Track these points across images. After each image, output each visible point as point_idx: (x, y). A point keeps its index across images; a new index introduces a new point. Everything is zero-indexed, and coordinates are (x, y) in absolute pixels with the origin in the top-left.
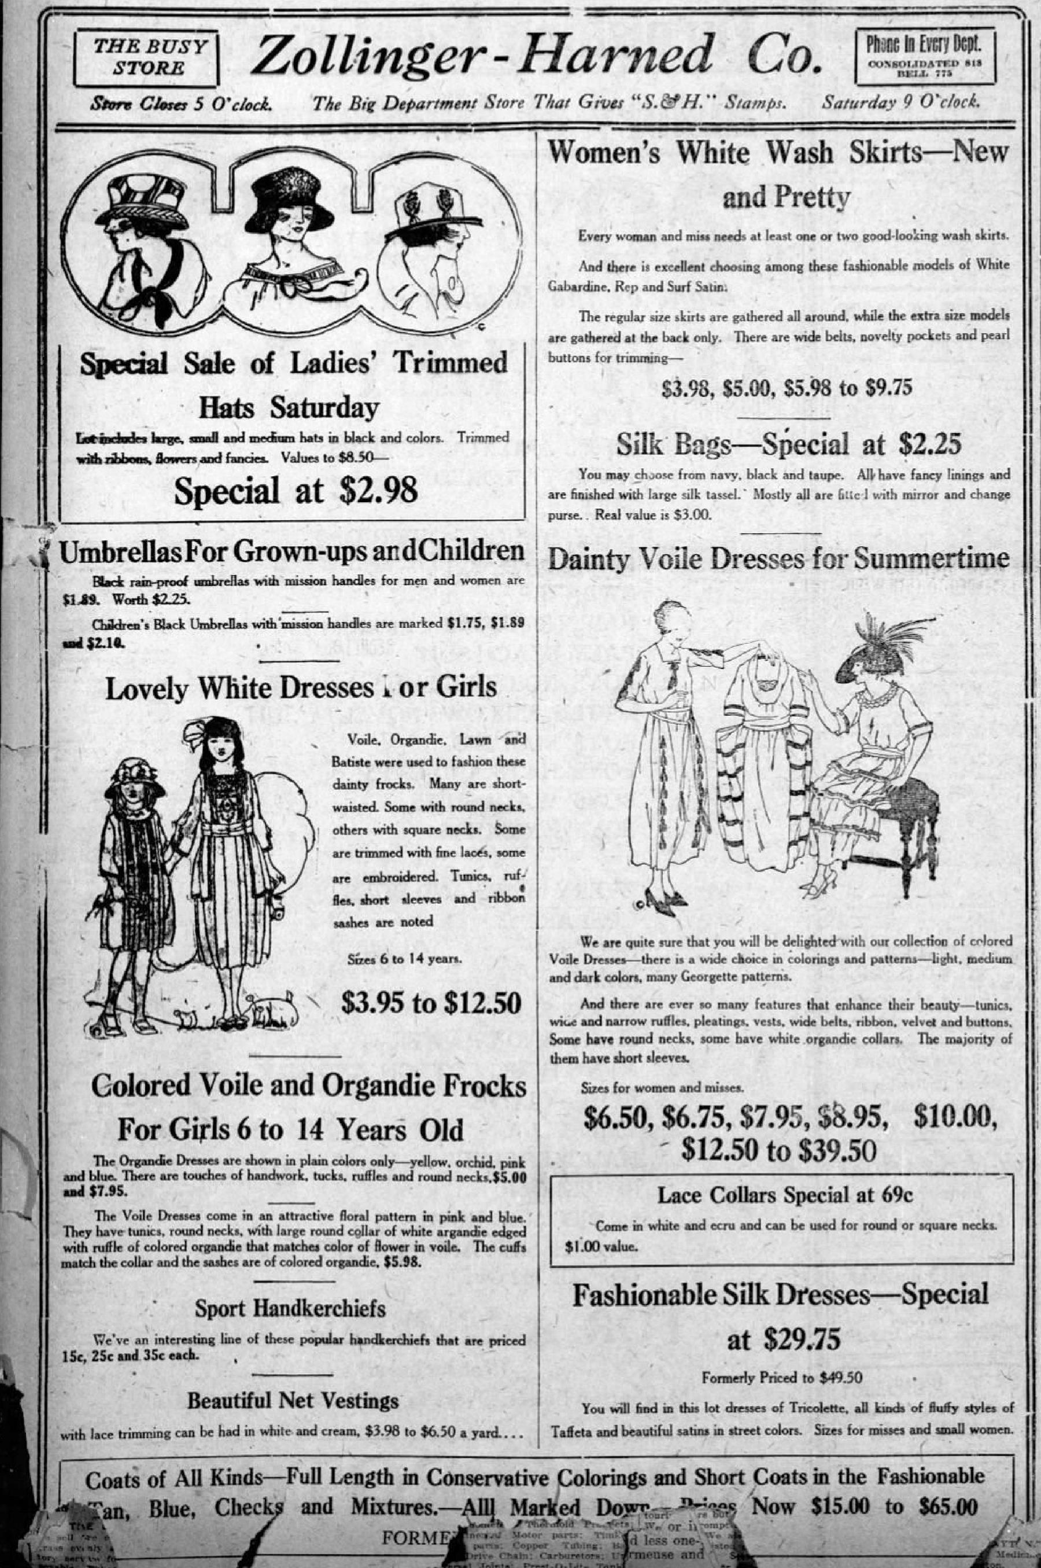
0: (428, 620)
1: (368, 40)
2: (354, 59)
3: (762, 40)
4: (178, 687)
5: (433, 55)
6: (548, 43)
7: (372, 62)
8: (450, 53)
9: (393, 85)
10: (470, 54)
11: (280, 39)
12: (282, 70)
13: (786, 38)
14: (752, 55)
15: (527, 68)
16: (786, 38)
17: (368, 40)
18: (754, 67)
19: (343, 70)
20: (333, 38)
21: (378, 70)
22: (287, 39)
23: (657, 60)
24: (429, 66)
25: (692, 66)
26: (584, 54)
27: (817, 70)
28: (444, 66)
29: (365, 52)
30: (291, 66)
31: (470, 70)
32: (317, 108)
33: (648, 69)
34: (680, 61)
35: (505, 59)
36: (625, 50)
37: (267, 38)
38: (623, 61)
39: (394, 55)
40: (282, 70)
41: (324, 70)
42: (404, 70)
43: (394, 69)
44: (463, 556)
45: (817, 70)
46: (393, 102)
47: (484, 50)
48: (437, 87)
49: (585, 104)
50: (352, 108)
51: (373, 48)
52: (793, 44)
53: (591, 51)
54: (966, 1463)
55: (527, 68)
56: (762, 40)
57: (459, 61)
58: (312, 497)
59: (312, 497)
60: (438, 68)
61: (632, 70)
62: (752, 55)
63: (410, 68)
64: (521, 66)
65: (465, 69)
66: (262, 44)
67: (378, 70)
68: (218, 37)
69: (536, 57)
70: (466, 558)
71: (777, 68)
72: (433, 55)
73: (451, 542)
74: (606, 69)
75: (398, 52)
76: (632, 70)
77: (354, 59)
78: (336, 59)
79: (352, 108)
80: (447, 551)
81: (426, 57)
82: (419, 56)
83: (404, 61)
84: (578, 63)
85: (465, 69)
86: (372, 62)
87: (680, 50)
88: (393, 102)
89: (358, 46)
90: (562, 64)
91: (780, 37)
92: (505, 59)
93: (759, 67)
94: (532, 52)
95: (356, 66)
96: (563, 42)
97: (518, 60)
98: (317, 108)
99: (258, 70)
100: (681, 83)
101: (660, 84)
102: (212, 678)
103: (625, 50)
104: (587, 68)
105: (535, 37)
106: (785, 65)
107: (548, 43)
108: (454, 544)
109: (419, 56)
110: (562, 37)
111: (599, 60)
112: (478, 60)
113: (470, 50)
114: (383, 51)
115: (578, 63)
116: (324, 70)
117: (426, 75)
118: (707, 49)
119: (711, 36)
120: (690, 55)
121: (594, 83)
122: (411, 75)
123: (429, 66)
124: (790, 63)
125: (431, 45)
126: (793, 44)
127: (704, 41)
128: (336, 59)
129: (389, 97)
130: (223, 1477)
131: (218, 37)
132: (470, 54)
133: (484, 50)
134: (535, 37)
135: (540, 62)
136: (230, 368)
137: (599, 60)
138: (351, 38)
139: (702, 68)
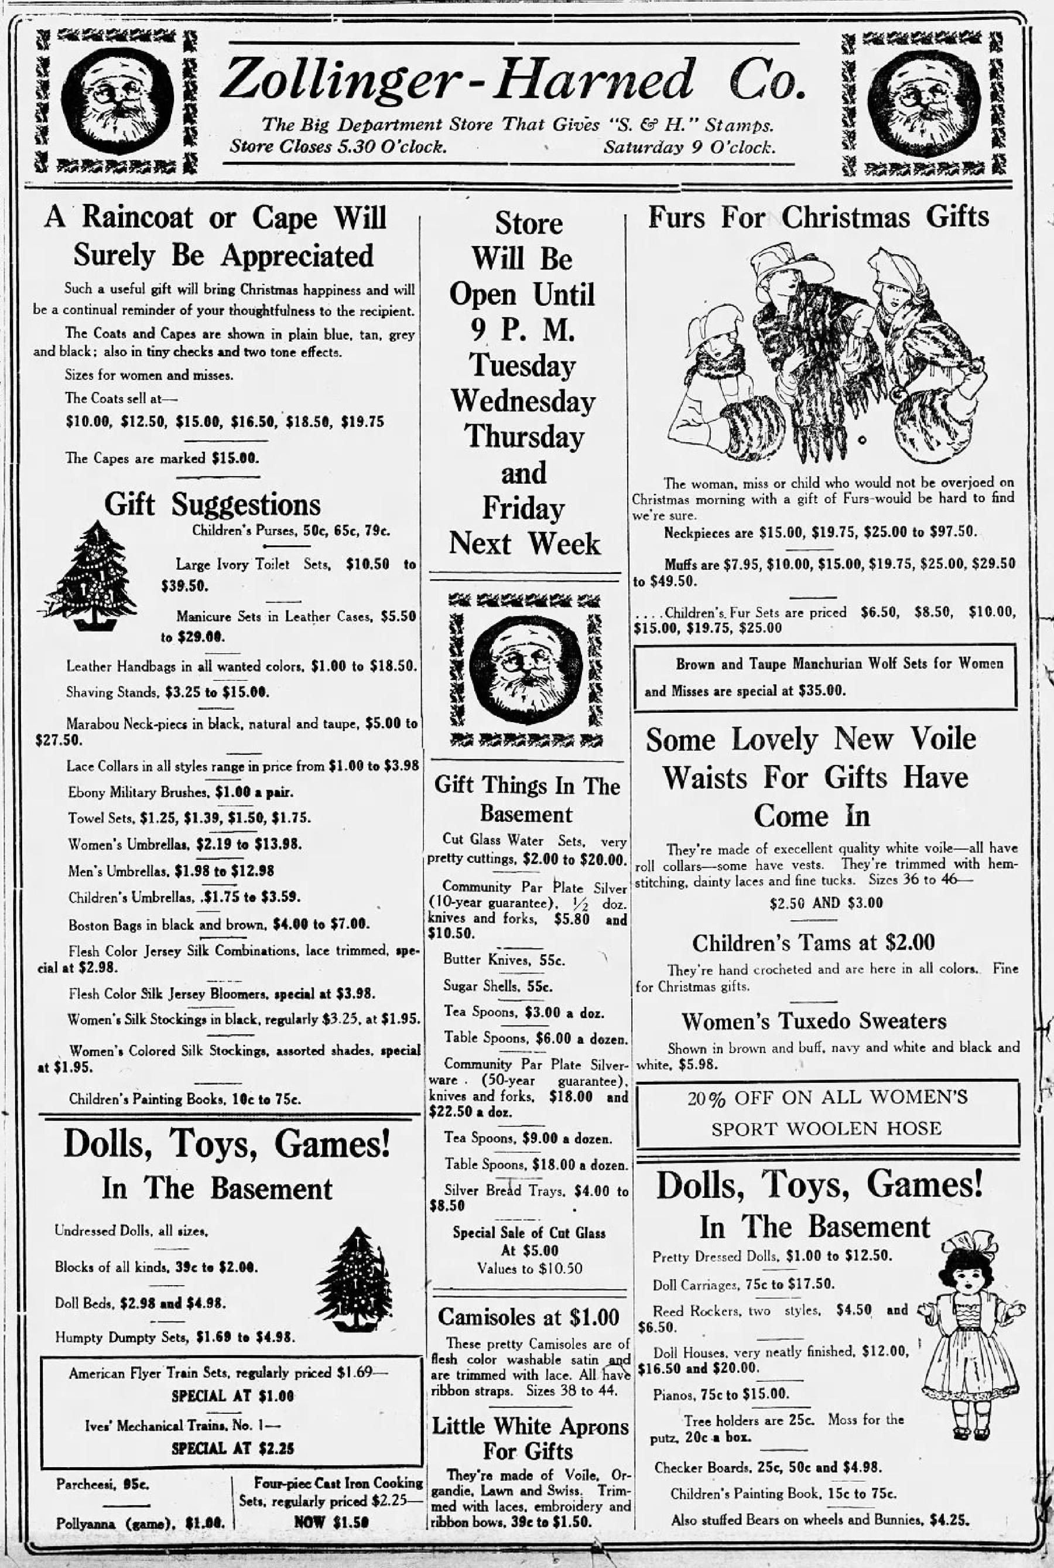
0: (837, 1348)
1: (339, 64)
2: (325, 84)
3: (741, 68)
4: (144, 253)
5: (407, 79)
6: (524, 68)
7: (344, 86)
8: (424, 77)
9: (362, 108)
10: (445, 78)
11: (249, 62)
12: (251, 94)
13: (769, 63)
14: (735, 78)
15: (503, 94)
16: (769, 63)
17: (339, 64)
18: (735, 89)
19: (314, 94)
20: (304, 61)
21: (350, 95)
22: (256, 61)
23: (637, 86)
24: (402, 91)
25: (553, 92)
26: (562, 79)
27: (801, 95)
28: (418, 91)
29: (337, 76)
30: (260, 89)
31: (589, 94)
32: (268, 129)
33: (628, 95)
34: (661, 86)
35: (481, 83)
36: (603, 75)
37: (236, 60)
38: (600, 87)
39: (366, 78)
40: (251, 94)
41: (295, 94)
42: (377, 94)
43: (366, 94)
44: (727, 948)
45: (801, 95)
46: (347, 124)
47: (459, 75)
48: (410, 110)
49: (559, 126)
50: (303, 129)
51: (345, 72)
52: (775, 70)
53: (570, 76)
54: (255, 277)
55: (503, 94)
56: (741, 68)
57: (434, 86)
58: (184, 222)
59: (184, 222)
60: (412, 93)
61: (611, 95)
62: (735, 78)
63: (384, 93)
64: (497, 92)
65: (439, 95)
66: (230, 67)
67: (350, 95)
68: (1019, 1085)
69: (512, 81)
70: (730, 950)
71: (760, 93)
72: (407, 79)
73: (718, 937)
74: (584, 95)
75: (371, 76)
76: (611, 95)
77: (325, 84)
78: (307, 82)
79: (303, 129)
80: (811, 218)
81: (399, 81)
82: (392, 80)
83: (377, 85)
84: (556, 89)
85: (439, 95)
86: (344, 86)
87: (660, 75)
88: (347, 124)
89: (330, 69)
90: (540, 90)
91: (763, 62)
92: (481, 83)
93: (741, 91)
94: (508, 76)
95: (308, 90)
96: (541, 66)
97: (494, 85)
98: (268, 129)
99: (226, 93)
100: (659, 108)
101: (636, 108)
102: (487, 248)
103: (603, 75)
104: (564, 93)
105: (512, 62)
106: (767, 90)
107: (524, 68)
108: (721, 940)
109: (392, 80)
110: (539, 62)
111: (576, 85)
112: (453, 84)
113: (445, 75)
114: (355, 75)
115: (556, 89)
116: (295, 94)
117: (399, 100)
118: (688, 75)
119: (692, 61)
120: (671, 79)
121: (573, 107)
122: (384, 100)
123: (402, 91)
124: (774, 91)
125: (405, 70)
126: (775, 70)
127: (684, 66)
128: (307, 82)
129: (344, 120)
130: (496, 959)
131: (1019, 1085)
132: (445, 78)
133: (459, 75)
134: (512, 62)
135: (517, 87)
136: (480, 1430)
137: (576, 85)
138: (323, 61)
139: (683, 93)
